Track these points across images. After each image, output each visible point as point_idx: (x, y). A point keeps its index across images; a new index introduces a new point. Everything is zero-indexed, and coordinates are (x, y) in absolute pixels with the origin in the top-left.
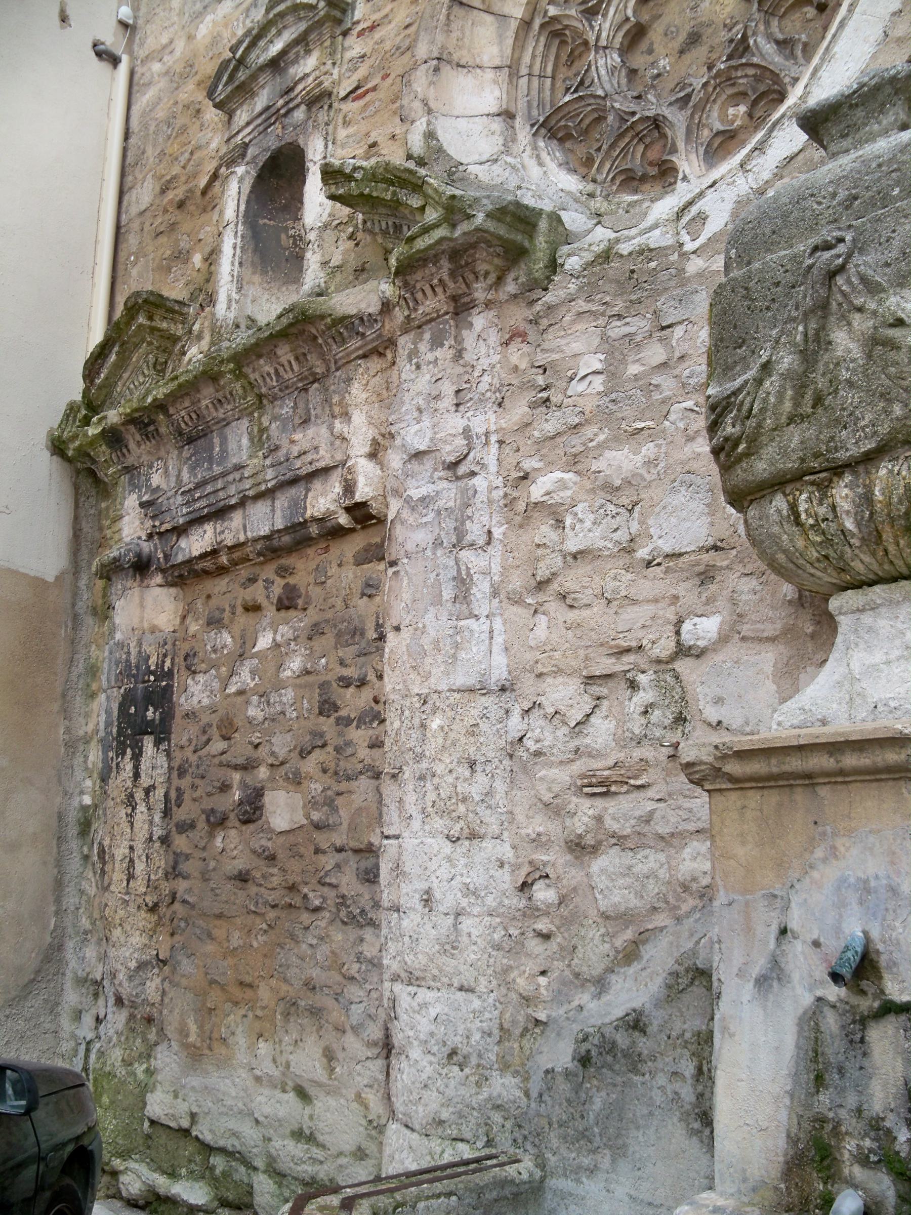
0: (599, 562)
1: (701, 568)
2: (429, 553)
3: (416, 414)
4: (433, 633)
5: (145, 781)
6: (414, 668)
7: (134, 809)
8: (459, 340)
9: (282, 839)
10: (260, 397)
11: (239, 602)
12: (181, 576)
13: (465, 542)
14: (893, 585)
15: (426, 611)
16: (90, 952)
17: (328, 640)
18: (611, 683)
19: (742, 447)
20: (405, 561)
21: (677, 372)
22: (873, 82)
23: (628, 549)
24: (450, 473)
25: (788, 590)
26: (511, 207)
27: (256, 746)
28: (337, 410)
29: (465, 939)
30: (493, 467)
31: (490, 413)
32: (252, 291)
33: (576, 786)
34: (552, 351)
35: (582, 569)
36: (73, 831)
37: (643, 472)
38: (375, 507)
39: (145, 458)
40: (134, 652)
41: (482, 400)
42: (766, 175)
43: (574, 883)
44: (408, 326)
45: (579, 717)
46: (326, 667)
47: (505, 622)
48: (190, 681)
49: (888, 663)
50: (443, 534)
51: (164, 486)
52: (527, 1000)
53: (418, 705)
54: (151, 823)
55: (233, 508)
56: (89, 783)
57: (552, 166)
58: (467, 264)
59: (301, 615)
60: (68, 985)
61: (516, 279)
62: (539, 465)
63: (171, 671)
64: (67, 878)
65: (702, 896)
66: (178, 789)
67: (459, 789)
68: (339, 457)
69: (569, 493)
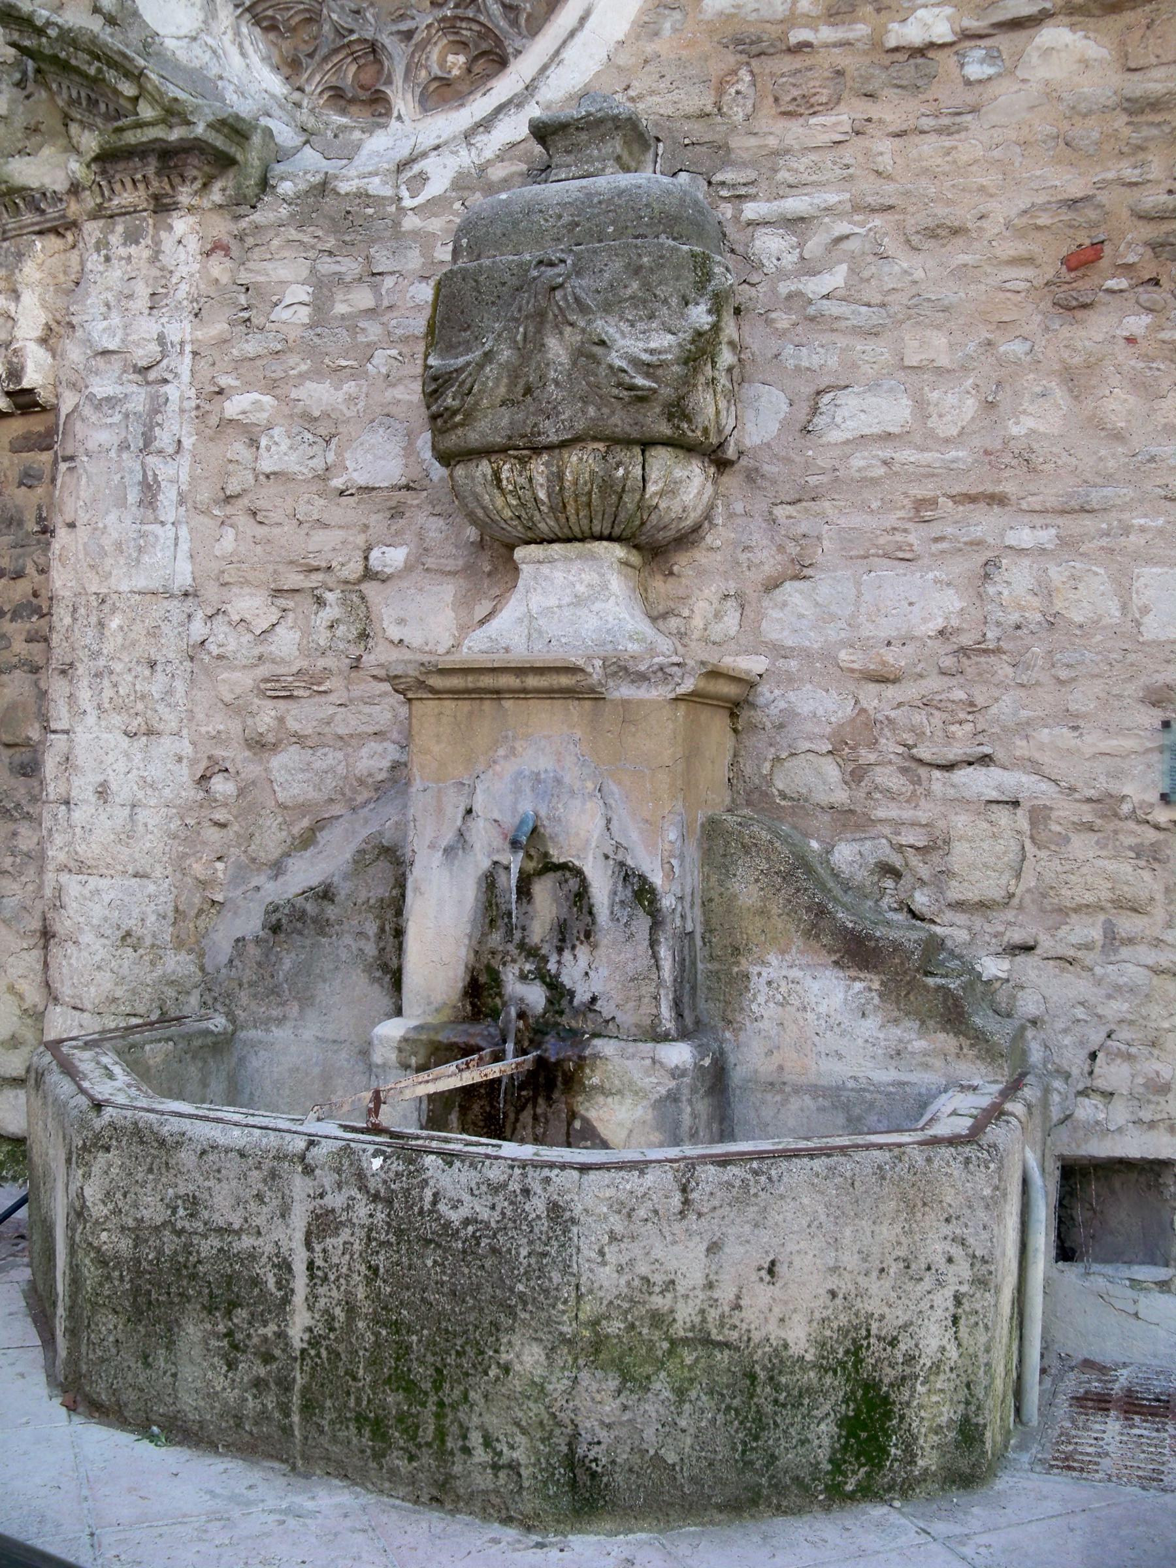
1: (393, 503)
3: (104, 309)
4: (115, 535)
6: (92, 567)
13: (152, 448)
14: (569, 545)
15: (107, 512)
18: (297, 597)
19: (458, 418)
20: (85, 459)
21: (385, 319)
22: (599, 115)
23: (324, 475)
25: (471, 533)
26: (231, 120)
29: (141, 828)
30: (186, 377)
31: (186, 322)
33: (258, 688)
34: (258, 272)
35: (272, 489)
37: (343, 408)
41: (178, 307)
42: (488, 154)
43: (252, 776)
44: (96, 214)
45: (265, 626)
47: (191, 531)
49: (559, 607)
50: (130, 438)
52: (203, 884)
53: (95, 604)
57: (255, 59)
58: (176, 166)
61: (223, 190)
62: (237, 383)
65: (377, 790)
67: (138, 687)
69: (265, 415)
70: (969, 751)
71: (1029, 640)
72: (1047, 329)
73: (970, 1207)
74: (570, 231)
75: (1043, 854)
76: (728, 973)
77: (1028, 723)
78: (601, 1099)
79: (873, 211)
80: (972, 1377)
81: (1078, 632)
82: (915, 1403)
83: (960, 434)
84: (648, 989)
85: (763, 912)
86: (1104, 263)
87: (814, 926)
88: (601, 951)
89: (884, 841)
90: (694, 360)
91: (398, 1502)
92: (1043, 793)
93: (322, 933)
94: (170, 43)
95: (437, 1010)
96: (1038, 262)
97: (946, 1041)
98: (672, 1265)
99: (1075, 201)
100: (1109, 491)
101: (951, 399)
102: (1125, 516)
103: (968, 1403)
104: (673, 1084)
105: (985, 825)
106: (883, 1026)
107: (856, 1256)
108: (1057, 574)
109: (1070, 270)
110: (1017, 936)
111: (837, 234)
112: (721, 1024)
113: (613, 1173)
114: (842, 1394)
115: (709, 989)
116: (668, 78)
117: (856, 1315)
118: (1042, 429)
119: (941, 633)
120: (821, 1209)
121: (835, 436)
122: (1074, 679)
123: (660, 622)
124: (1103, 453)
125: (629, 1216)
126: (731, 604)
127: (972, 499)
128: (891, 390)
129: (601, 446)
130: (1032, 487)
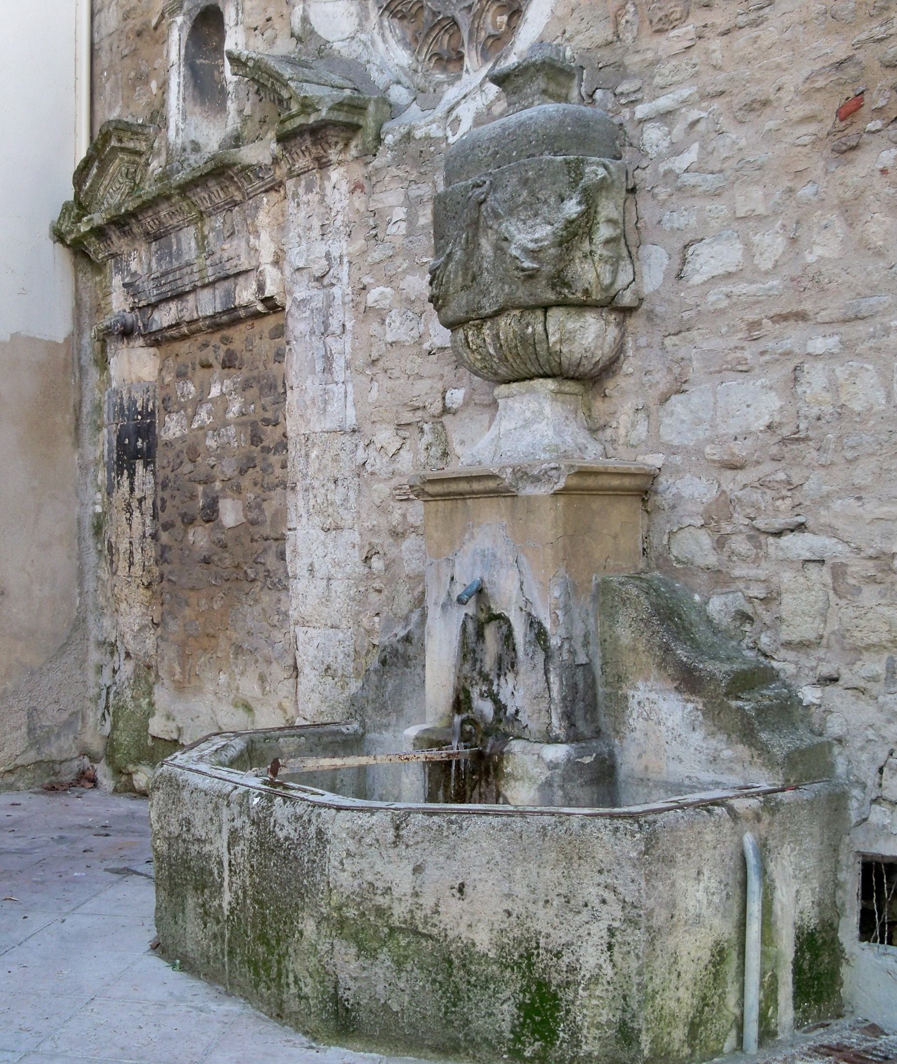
0: (403, 350)
2: (307, 338)
5: (138, 494)
7: (131, 514)
8: (322, 188)
9: (230, 533)
10: (201, 213)
11: (197, 362)
12: (157, 340)
13: (329, 332)
15: (307, 378)
16: (107, 622)
17: (254, 391)
18: (411, 429)
24: (318, 284)
27: (213, 467)
28: (251, 228)
29: (333, 594)
30: (345, 280)
32: (194, 120)
36: (88, 533)
38: (279, 300)
39: (125, 249)
40: (126, 397)
41: (338, 231)
44: (290, 174)
45: (394, 451)
46: (254, 411)
48: (167, 418)
51: (140, 272)
54: (144, 524)
55: (189, 292)
56: (99, 496)
57: (392, 42)
59: (238, 372)
60: (92, 646)
62: (372, 281)
63: (153, 412)
64: (86, 568)
66: (162, 499)
68: (254, 263)
69: (388, 301)
70: (788, 520)
71: (826, 429)
72: (827, 172)
73: (619, 864)
74: (494, 158)
75: (843, 602)
76: (616, 694)
77: (828, 495)
78: (512, 783)
79: (713, 97)
80: (627, 992)
81: (858, 419)
82: (578, 1003)
83: (775, 267)
84: (544, 705)
85: (634, 649)
86: (864, 110)
87: (664, 660)
88: (521, 677)
89: (740, 594)
90: (567, 242)
91: (262, 1015)
92: (840, 552)
93: (407, 666)
94: (337, 46)
95: (441, 718)
96: (819, 118)
97: (743, 751)
98: (389, 877)
99: (841, 63)
100: (873, 301)
101: (767, 239)
102: (885, 320)
103: (624, 1011)
104: (548, 773)
105: (802, 580)
106: (705, 738)
107: (526, 889)
108: (841, 373)
109: (842, 120)
110: (825, 670)
111: (690, 120)
112: (613, 734)
113: (355, 813)
114: (519, 986)
115: (606, 707)
116: (585, 21)
117: (528, 930)
118: (827, 255)
119: (769, 427)
120: (497, 852)
121: (697, 279)
122: (856, 459)
123: (600, 433)
124: (870, 268)
125: (360, 841)
126: (641, 415)
127: (785, 318)
128: (728, 238)
129: (517, 312)
130: (822, 304)
